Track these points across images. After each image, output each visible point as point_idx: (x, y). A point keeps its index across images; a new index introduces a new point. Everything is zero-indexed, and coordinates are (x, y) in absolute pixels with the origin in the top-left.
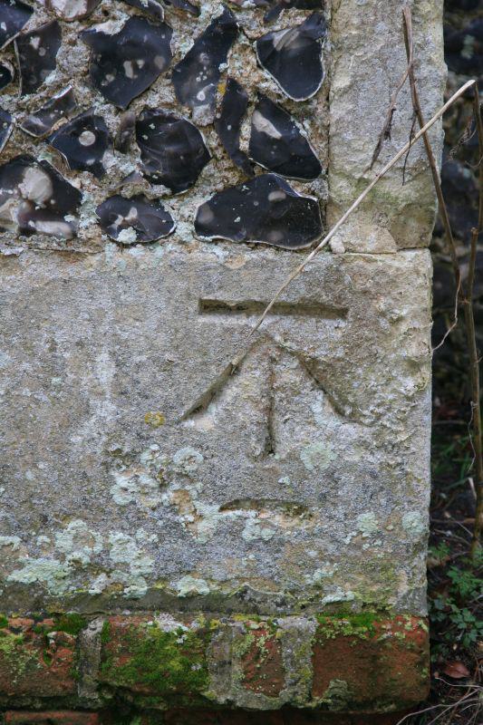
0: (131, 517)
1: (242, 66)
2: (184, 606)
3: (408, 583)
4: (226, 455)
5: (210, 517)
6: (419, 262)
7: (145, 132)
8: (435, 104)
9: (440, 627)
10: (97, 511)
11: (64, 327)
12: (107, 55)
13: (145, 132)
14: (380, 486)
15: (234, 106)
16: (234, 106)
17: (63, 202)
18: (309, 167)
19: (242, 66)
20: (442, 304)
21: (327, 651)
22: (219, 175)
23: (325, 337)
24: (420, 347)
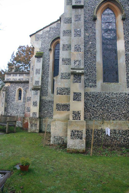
0: (77, 147)
1: (80, 135)
2: (79, 149)
3: (85, 149)
4: (8, 97)
5: (79, 147)
6: (85, 140)
7: (78, 136)
8: (85, 136)
9: (86, 150)
10: (77, 147)
11: (76, 142)
12: (77, 135)
13: (78, 136)
14: (84, 146)
15: (80, 136)
16: (80, 136)
17: (76, 138)
18: (82, 137)
19: (80, 135)
20: (86, 142)
21: (83, 151)
22: (80, 138)
23: (83, 142)
24: (85, 142)
